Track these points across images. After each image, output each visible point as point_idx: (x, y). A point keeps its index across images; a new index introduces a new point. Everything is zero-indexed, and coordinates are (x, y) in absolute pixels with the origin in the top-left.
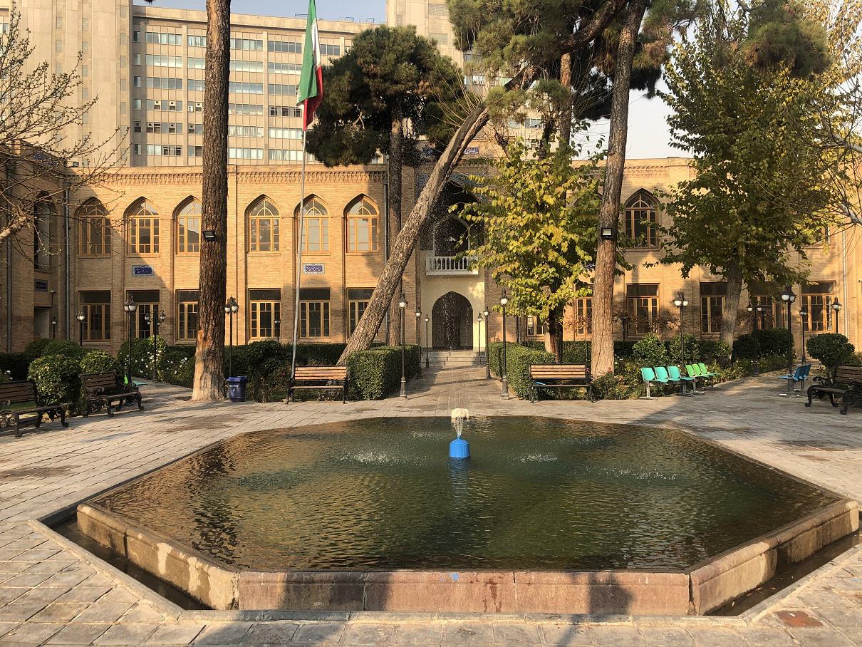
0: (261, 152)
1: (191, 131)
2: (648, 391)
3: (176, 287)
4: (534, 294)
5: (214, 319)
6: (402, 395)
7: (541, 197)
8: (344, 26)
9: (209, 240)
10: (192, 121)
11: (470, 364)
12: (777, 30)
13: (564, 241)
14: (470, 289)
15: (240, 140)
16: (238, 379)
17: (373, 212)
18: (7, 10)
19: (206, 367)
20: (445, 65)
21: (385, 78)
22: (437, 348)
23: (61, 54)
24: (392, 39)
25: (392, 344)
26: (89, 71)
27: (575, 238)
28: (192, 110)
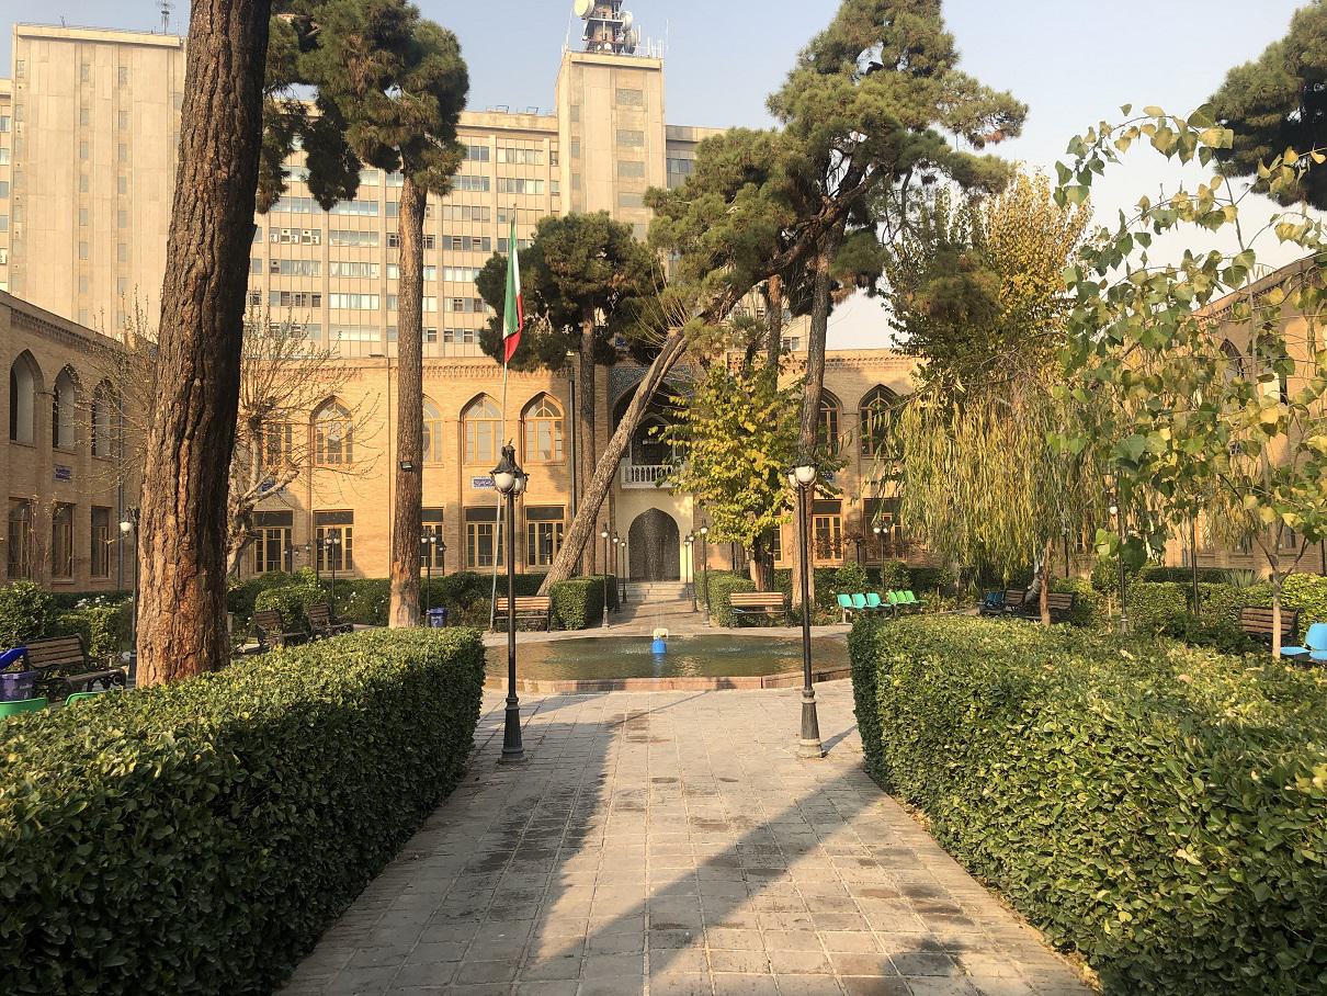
0: (375, 300)
1: (274, 270)
2: (844, 616)
3: (314, 507)
4: (737, 521)
5: (411, 551)
6: (605, 624)
7: (743, 423)
8: (495, 119)
9: (406, 470)
10: (275, 256)
11: (677, 598)
12: (945, 287)
13: (765, 468)
14: (677, 504)
15: (345, 283)
16: (440, 611)
17: (557, 413)
18: (9, 97)
19: (403, 599)
20: (642, 254)
21: (576, 277)
22: (633, 579)
23: (86, 162)
24: (583, 231)
25: (586, 573)
26: (129, 186)
27: (776, 464)
28: (276, 240)
